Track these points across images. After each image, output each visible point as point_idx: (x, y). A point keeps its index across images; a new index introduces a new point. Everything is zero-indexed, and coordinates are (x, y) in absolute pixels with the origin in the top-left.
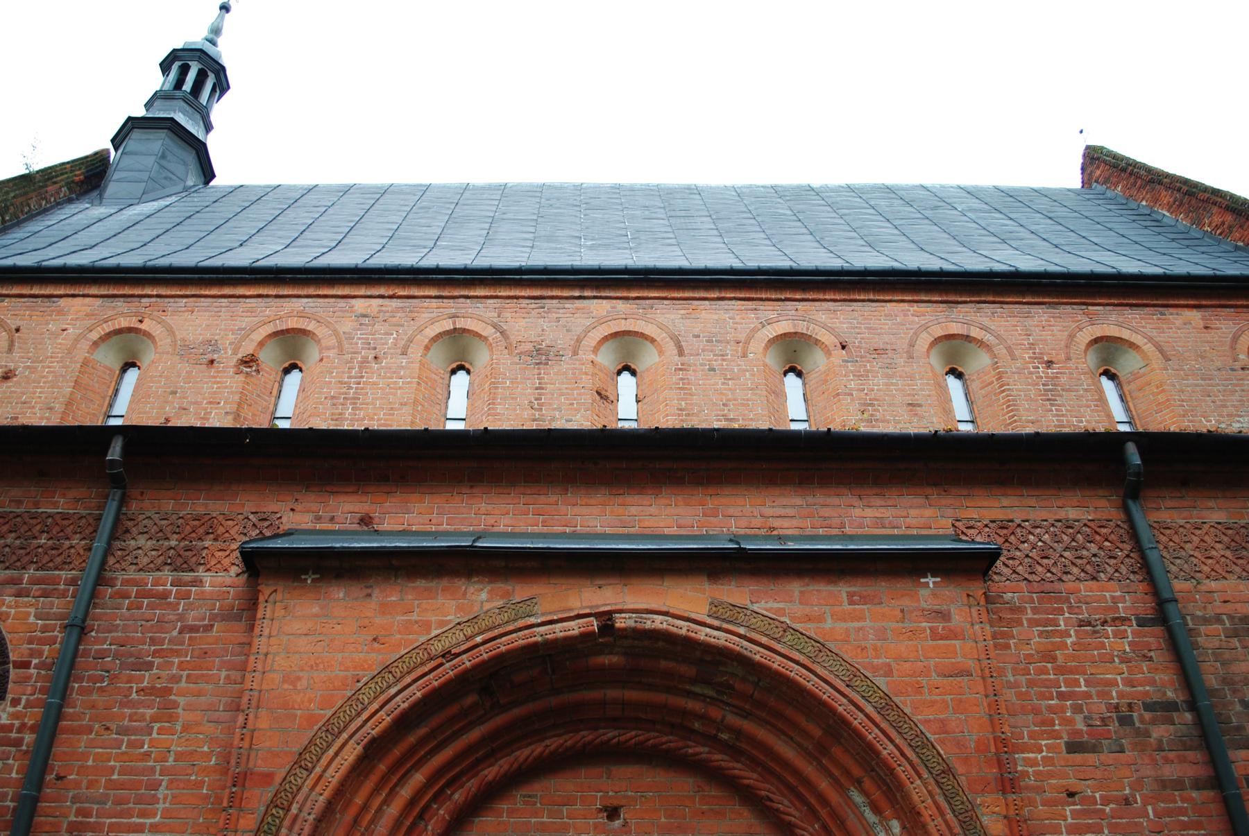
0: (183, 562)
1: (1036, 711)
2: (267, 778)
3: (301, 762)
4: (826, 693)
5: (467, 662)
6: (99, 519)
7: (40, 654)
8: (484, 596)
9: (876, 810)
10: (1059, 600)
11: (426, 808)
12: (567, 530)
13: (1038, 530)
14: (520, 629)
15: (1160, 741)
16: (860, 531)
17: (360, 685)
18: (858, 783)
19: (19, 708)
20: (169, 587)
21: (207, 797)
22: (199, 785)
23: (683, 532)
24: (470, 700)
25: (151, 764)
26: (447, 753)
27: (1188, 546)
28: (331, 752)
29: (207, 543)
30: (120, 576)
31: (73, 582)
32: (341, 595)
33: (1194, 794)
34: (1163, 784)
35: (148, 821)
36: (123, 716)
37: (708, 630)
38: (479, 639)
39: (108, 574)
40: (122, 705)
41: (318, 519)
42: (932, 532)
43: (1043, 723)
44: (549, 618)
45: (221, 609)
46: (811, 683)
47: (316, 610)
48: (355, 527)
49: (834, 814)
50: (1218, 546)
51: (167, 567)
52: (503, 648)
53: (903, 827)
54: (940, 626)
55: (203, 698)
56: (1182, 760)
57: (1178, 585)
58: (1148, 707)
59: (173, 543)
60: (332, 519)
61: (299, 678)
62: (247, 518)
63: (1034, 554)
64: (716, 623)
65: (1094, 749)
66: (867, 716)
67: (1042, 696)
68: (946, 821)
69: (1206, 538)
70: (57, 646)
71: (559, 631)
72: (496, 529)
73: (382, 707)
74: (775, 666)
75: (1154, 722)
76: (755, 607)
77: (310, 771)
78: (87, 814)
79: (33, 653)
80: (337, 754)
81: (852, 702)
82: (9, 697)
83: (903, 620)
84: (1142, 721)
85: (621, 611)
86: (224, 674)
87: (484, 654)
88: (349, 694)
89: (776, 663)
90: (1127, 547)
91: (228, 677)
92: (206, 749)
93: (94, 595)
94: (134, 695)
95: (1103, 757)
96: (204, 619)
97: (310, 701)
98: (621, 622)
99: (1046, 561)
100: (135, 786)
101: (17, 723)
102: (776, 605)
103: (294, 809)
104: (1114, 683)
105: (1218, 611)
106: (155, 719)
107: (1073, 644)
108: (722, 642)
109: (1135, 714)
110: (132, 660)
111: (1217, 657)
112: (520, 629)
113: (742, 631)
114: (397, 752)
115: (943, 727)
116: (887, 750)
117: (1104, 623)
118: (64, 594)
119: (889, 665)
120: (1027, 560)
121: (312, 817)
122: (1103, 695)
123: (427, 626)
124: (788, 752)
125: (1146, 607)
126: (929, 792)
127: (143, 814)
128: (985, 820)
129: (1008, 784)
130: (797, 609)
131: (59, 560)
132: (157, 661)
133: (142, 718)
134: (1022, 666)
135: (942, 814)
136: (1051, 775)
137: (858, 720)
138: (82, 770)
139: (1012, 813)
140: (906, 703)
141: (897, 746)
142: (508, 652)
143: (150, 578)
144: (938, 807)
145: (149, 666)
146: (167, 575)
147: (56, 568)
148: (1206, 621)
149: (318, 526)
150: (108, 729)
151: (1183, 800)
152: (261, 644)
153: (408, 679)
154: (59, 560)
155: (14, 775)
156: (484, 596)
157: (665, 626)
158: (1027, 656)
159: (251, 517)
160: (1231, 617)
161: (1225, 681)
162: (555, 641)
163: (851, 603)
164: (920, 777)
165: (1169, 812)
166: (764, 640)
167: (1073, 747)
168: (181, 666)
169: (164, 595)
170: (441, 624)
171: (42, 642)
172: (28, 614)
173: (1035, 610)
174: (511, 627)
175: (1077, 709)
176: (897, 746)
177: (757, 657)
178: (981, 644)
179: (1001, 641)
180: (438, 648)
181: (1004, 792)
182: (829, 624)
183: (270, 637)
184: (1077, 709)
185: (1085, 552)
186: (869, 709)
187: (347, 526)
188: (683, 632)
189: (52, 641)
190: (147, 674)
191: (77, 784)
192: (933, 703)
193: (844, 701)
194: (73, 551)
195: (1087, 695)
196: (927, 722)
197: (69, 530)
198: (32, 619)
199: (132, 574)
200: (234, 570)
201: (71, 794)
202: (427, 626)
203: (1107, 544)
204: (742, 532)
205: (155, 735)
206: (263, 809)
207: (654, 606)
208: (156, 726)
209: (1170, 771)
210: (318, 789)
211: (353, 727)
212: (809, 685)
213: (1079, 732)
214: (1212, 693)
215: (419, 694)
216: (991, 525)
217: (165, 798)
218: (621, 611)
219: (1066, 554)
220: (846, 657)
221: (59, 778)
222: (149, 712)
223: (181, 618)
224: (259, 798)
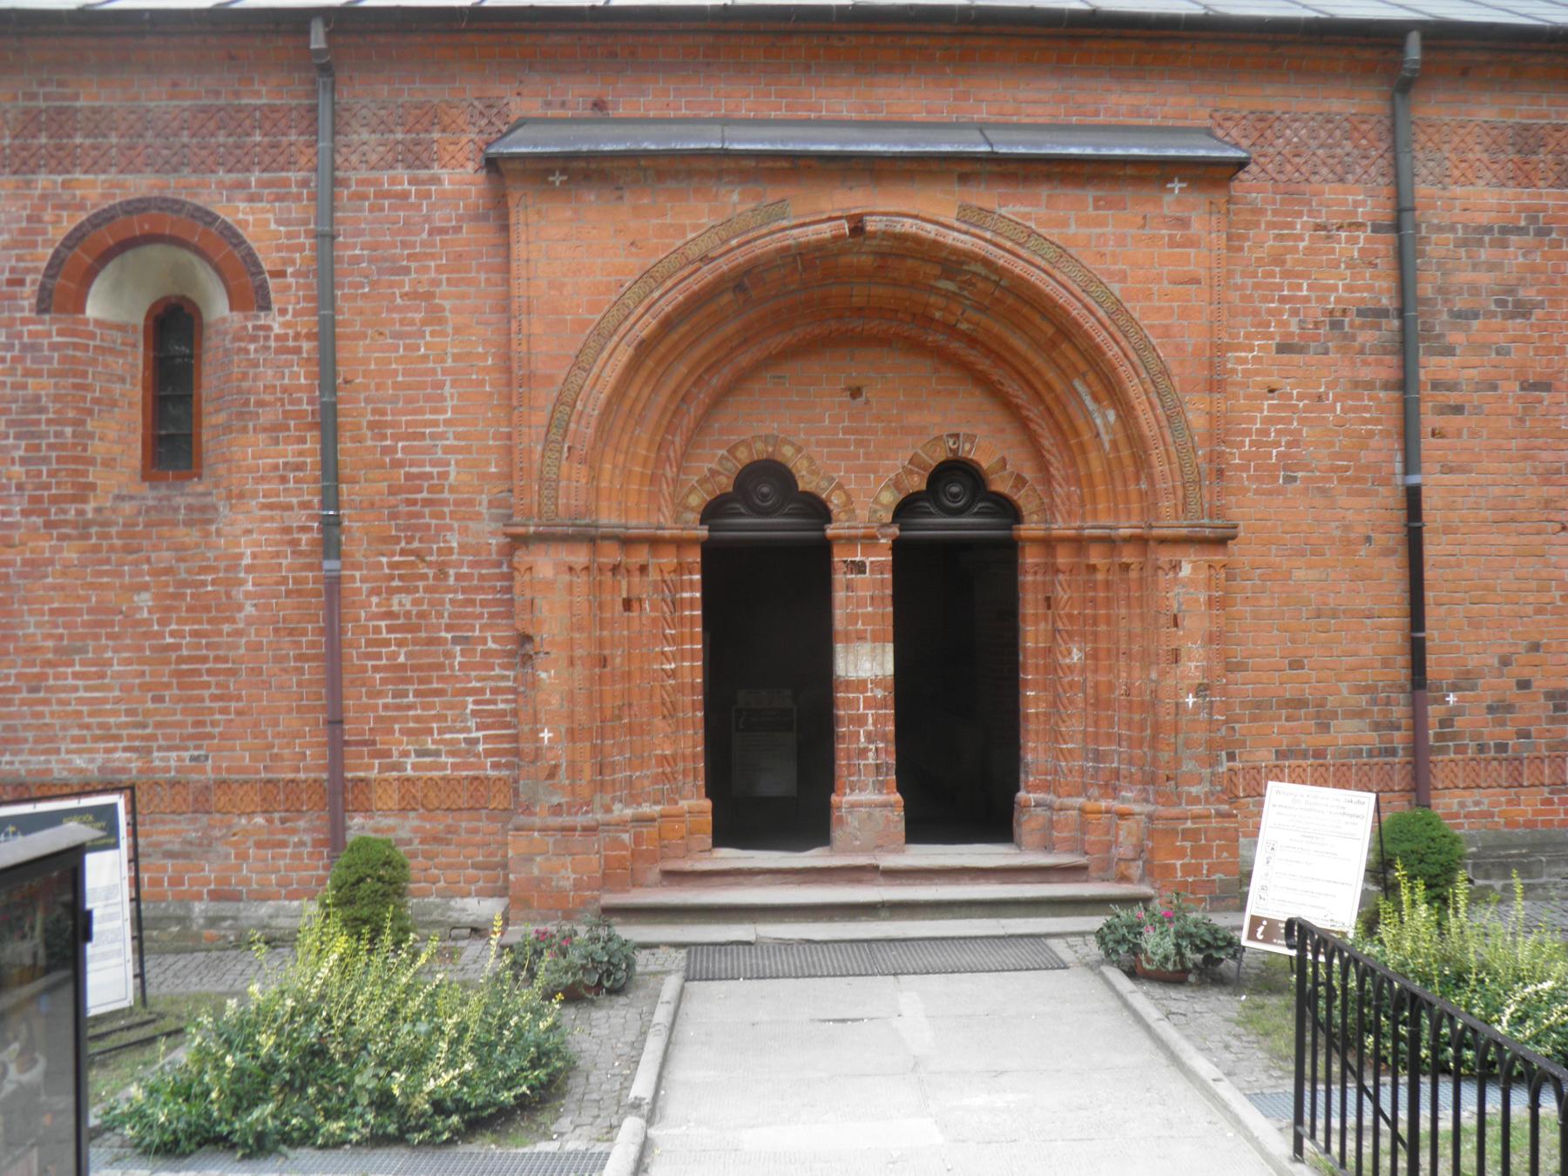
0: (416, 157)
1: (1256, 313)
2: (550, 379)
3: (580, 363)
4: (1062, 298)
5: (724, 265)
6: (313, 109)
7: (293, 262)
8: (735, 197)
9: (1095, 398)
10: (1301, 202)
11: (688, 392)
12: (813, 115)
13: (1297, 125)
14: (773, 233)
15: (1363, 347)
16: (1113, 120)
17: (623, 290)
18: (1083, 376)
19: (289, 317)
20: (406, 186)
21: (491, 395)
22: (481, 383)
23: (933, 118)
24: (726, 298)
25: (431, 365)
26: (706, 345)
27: (1446, 147)
28: (605, 354)
29: (436, 135)
30: (354, 176)
31: (305, 183)
32: (592, 198)
33: (1382, 394)
34: (1356, 384)
35: (441, 417)
36: (392, 321)
37: (956, 234)
38: (734, 242)
39: (339, 174)
40: (389, 310)
41: (548, 104)
42: (1188, 123)
43: (1260, 325)
44: (802, 221)
45: (466, 207)
46: (1049, 287)
47: (569, 214)
48: (588, 113)
49: (1058, 399)
50: (1478, 148)
51: (400, 165)
52: (758, 252)
53: (1118, 416)
54: (1178, 233)
55: (468, 302)
56: (1379, 363)
57: (1422, 189)
58: (1360, 313)
59: (399, 136)
60: (563, 105)
61: (563, 285)
62: (471, 104)
63: (1286, 151)
64: (964, 227)
65: (1301, 350)
66: (1098, 320)
67: (1265, 299)
68: (1156, 417)
69: (1468, 139)
70: (307, 253)
71: (811, 234)
72: (737, 115)
73: (647, 311)
74: (1017, 270)
75: (1363, 327)
76: (1003, 211)
77: (588, 371)
78: (383, 413)
79: (286, 262)
80: (610, 355)
81: (1086, 307)
82: (275, 307)
83: (1143, 226)
84: (1352, 325)
85: (871, 214)
86: (483, 276)
87: (740, 257)
88: (614, 298)
89: (1019, 268)
90: (1383, 146)
91: (487, 280)
92: (480, 350)
93: (333, 197)
94: (399, 301)
95: (1307, 357)
96: (450, 220)
97: (578, 306)
98: (872, 224)
99: (1297, 160)
100: (421, 386)
101: (291, 332)
102: (1023, 209)
103: (579, 406)
104: (1334, 288)
105: (1455, 219)
106: (425, 323)
107: (1305, 248)
108: (968, 247)
109: (1347, 320)
110: (387, 265)
111: (1440, 266)
112: (773, 233)
113: (988, 235)
114: (662, 349)
115: (1166, 332)
116: (1112, 352)
117: (1340, 228)
118: (298, 198)
119: (1124, 272)
120: (1278, 158)
121: (596, 413)
122: (1323, 299)
123: (681, 230)
124: (1018, 342)
125: (1385, 214)
126: (1146, 391)
127: (434, 411)
128: (1190, 416)
129: (1216, 384)
130: (1042, 211)
131: (282, 159)
132: (413, 265)
133: (412, 323)
134: (1251, 269)
135: (1153, 408)
136: (1257, 373)
137: (1089, 324)
138: (366, 374)
139: (1214, 410)
140: (1135, 308)
141: (1122, 349)
142: (702, 289)
143: (385, 176)
144: (1150, 403)
145: (407, 270)
146: (401, 172)
147: (282, 169)
148: (1440, 229)
149: (549, 113)
150: (381, 334)
151: (1370, 399)
152: (519, 250)
153: (669, 283)
154: (282, 159)
155: (302, 381)
156: (735, 197)
157: (914, 230)
158: (1258, 259)
159: (476, 103)
160: (1466, 227)
161: (1440, 290)
162: (807, 245)
163: (1097, 208)
164: (1138, 376)
165: (1355, 409)
166: (1009, 244)
167: (1283, 348)
168: (438, 269)
169: (405, 195)
170: (695, 227)
171: (291, 248)
172: (267, 222)
173: (1275, 213)
174: (764, 230)
175: (1295, 312)
176: (1122, 349)
177: (1001, 262)
178: (1215, 253)
179: (1234, 242)
180: (695, 251)
181: (1211, 391)
182: (1072, 229)
183: (528, 243)
184: (1295, 312)
185: (1339, 151)
186: (1101, 313)
187: (579, 112)
188: (932, 236)
189: (301, 248)
190: (407, 279)
191: (366, 387)
192: (1160, 309)
193: (1079, 305)
194: (293, 149)
195: (1307, 300)
196: (1151, 327)
197: (282, 124)
198: (273, 226)
199: (364, 174)
200: (471, 166)
201: (362, 396)
202: (681, 230)
203: (1364, 142)
204: (993, 118)
205: (428, 338)
206: (550, 407)
207: (904, 209)
208: (428, 329)
209: (1366, 373)
210: (598, 387)
211: (622, 330)
212: (1048, 290)
213: (1292, 335)
214: (1425, 301)
215: (681, 298)
216: (1251, 117)
217: (452, 396)
218: (871, 214)
219: (1320, 152)
220: (1085, 263)
221: (346, 382)
222: (418, 316)
223: (428, 219)
224: (545, 398)
